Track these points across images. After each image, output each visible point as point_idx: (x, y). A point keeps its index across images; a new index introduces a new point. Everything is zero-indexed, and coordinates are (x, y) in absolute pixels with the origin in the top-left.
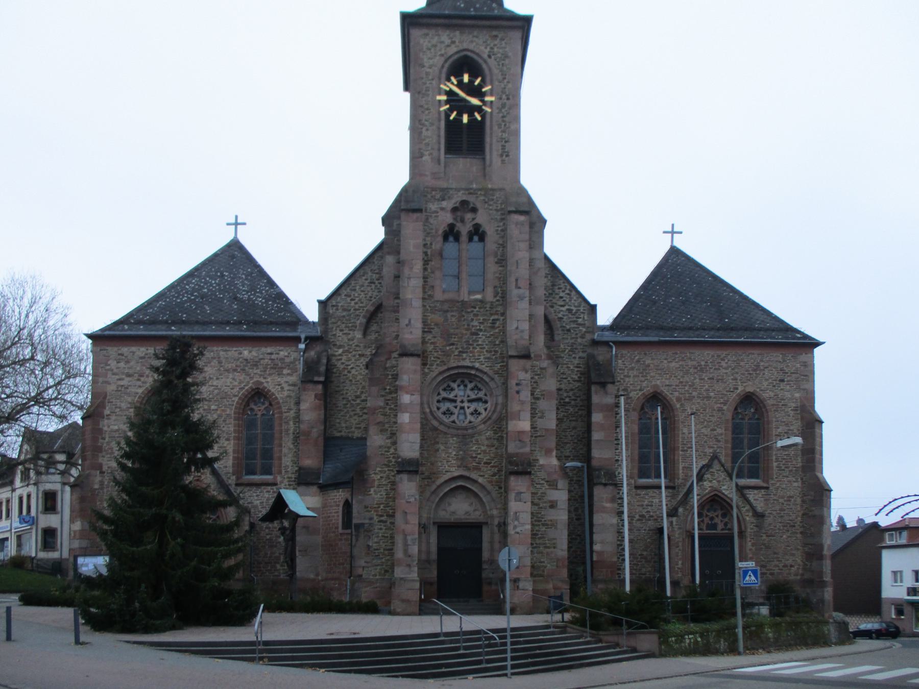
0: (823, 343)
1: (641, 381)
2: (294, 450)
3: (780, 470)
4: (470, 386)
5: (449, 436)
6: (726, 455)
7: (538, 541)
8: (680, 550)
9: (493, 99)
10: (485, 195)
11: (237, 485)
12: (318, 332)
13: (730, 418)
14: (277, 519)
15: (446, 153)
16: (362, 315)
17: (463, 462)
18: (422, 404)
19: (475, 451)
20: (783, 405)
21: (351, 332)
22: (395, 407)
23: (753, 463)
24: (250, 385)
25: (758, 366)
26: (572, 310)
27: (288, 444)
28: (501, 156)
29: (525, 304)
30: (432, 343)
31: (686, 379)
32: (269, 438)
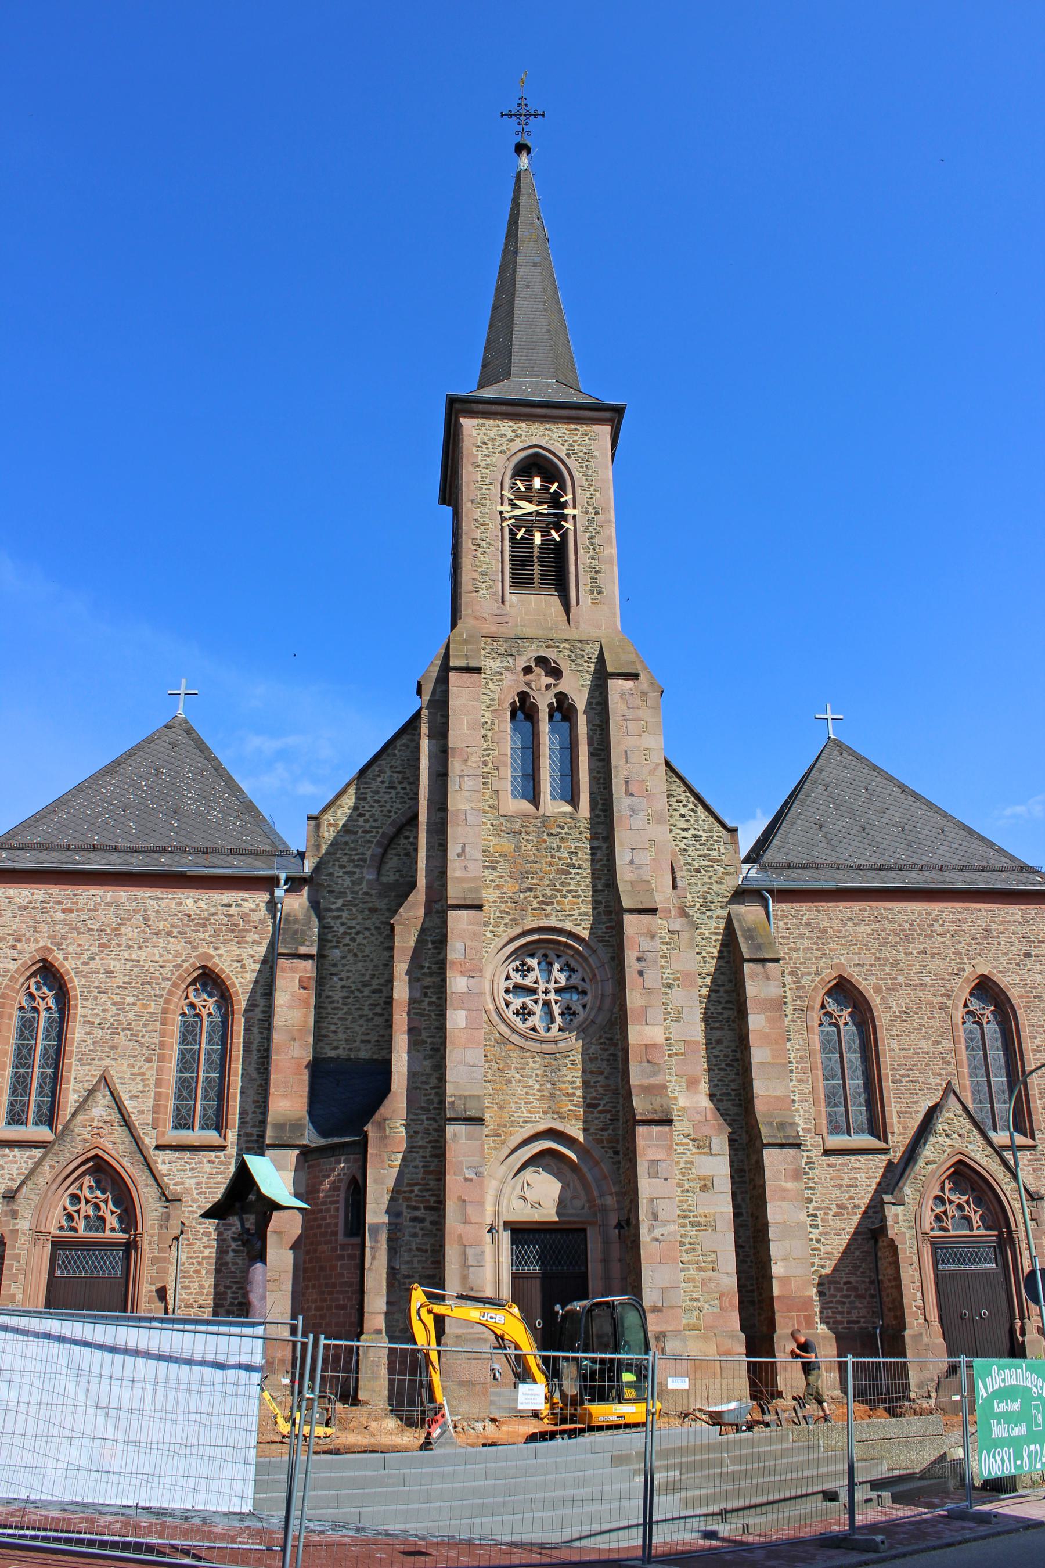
1: (816, 958)
2: (259, 1082)
5: (528, 1054)
11: (158, 1147)
16: (375, 840)
19: (571, 1083)
20: (1035, 997)
21: (357, 870)
24: (192, 960)
25: (988, 930)
31: (885, 953)
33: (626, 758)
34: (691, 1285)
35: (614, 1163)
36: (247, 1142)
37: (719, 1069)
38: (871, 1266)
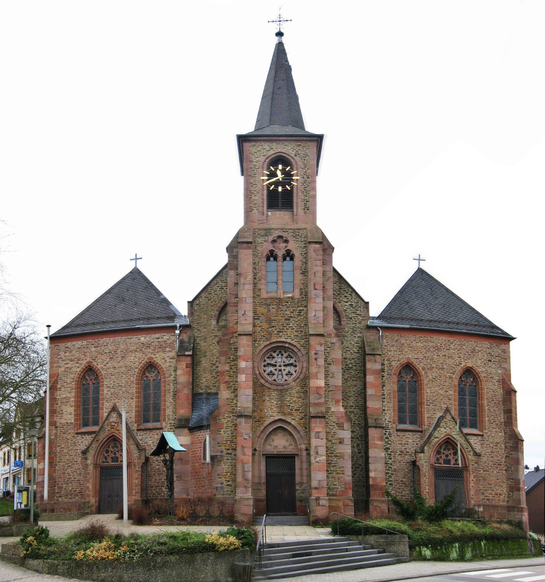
0: (515, 338)
1: (399, 355)
3: (490, 423)
4: (285, 355)
6: (455, 410)
7: (332, 469)
8: (427, 478)
9: (298, 178)
10: (293, 233)
11: (138, 430)
12: (187, 322)
13: (457, 384)
14: (162, 454)
15: (268, 209)
17: (281, 408)
18: (253, 368)
19: (289, 401)
20: (491, 377)
22: (235, 371)
23: (473, 417)
24: (146, 360)
26: (353, 305)
27: (169, 398)
28: (304, 209)
29: (320, 300)
30: (260, 326)
31: (428, 354)
32: (158, 396)
33: (315, 275)
34: (334, 479)
35: (305, 432)
36: (170, 426)
37: (355, 396)
38: (412, 475)
